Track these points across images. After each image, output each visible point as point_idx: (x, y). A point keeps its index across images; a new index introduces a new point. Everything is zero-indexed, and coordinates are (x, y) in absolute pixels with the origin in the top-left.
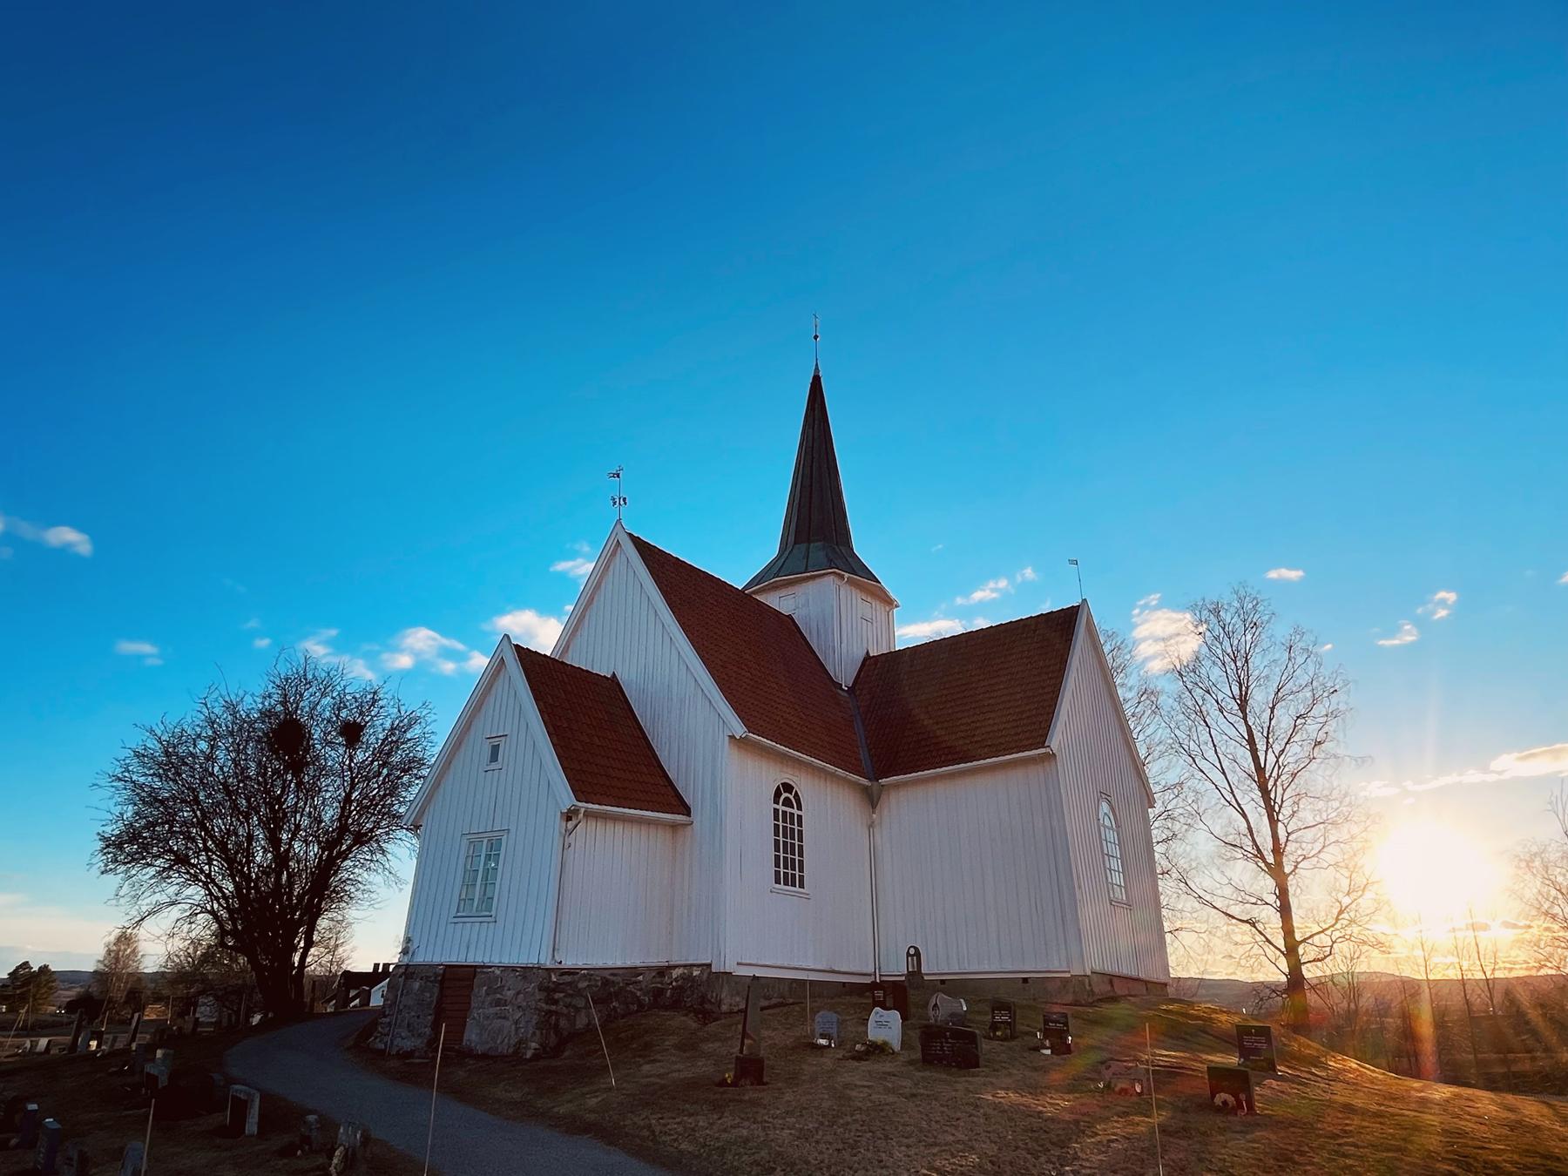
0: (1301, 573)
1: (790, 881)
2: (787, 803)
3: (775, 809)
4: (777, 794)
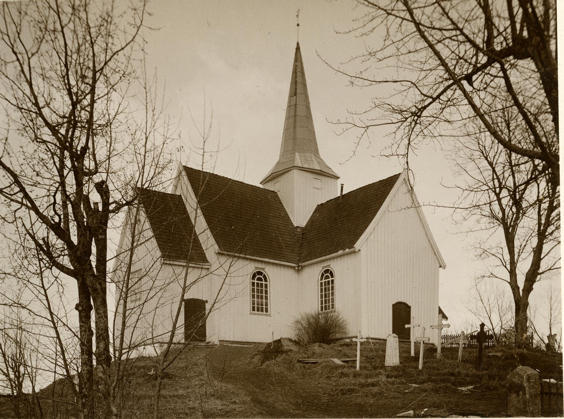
0: (527, 37)
1: (260, 309)
2: (259, 279)
3: (252, 282)
4: (254, 277)
